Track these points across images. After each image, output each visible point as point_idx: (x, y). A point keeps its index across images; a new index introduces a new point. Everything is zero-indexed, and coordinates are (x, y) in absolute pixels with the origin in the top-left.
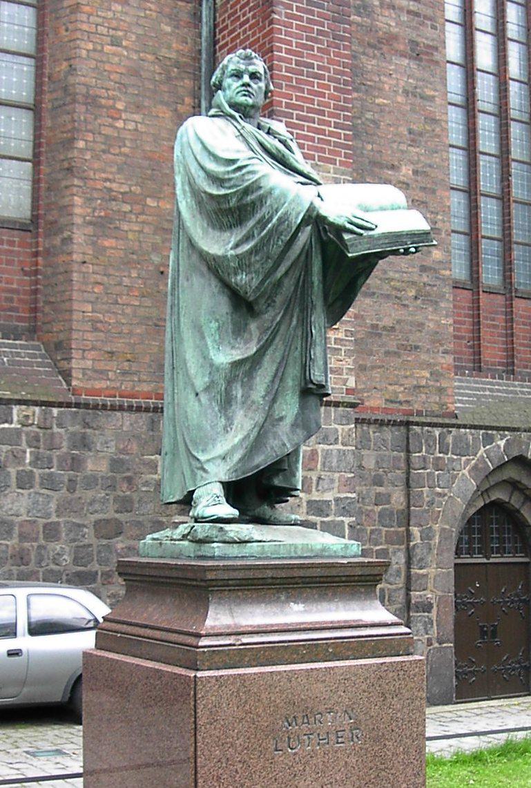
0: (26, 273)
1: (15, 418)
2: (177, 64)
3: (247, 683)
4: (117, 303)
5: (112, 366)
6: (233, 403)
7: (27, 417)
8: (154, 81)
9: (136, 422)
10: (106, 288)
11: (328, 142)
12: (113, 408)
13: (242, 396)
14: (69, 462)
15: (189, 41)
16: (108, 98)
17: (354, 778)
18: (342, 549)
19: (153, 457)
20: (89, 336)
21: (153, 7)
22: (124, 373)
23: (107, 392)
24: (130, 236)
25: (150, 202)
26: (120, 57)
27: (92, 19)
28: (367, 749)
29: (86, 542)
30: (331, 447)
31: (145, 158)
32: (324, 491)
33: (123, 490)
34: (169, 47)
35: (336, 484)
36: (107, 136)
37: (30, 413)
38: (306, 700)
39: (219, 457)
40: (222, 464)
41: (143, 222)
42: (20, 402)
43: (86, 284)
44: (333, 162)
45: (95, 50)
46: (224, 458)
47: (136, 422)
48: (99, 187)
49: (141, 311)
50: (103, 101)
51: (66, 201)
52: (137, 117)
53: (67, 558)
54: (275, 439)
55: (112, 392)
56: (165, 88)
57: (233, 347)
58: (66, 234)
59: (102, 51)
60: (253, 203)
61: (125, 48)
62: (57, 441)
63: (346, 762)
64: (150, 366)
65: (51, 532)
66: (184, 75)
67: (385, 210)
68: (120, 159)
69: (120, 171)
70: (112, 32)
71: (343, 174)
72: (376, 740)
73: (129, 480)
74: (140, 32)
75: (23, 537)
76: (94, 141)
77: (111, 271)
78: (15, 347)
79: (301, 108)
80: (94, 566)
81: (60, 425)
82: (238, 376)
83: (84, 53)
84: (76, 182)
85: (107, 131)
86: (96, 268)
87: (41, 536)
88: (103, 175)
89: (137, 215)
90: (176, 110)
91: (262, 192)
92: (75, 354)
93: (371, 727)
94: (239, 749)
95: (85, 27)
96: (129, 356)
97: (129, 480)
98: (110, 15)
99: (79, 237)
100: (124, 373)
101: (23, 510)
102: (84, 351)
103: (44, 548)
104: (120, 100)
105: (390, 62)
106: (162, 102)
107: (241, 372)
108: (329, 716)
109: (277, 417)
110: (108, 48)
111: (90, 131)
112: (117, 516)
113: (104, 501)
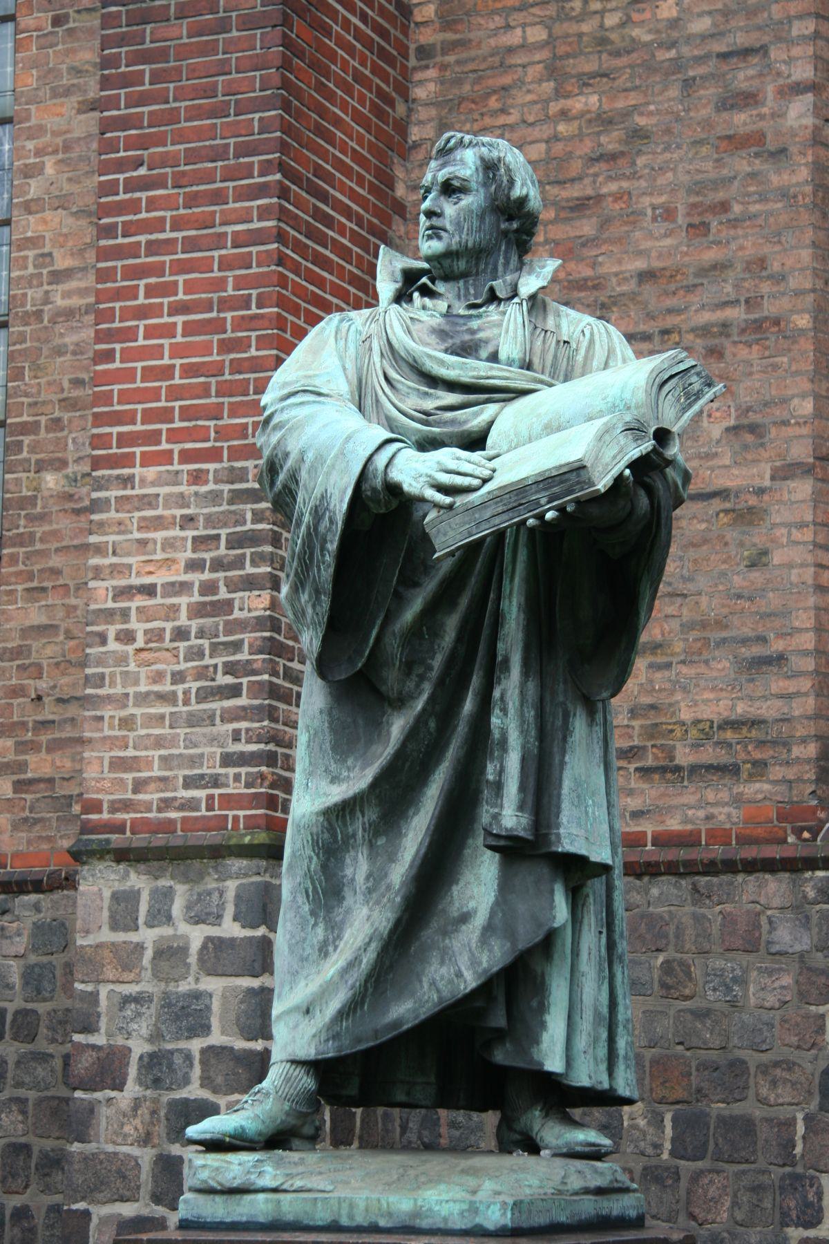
6: (347, 892)
13: (367, 878)
18: (462, 1213)
39: (296, 1009)
46: (308, 1011)
54: (442, 963)
57: (335, 780)
60: (285, 486)
67: (559, 429)
82: (354, 836)
107: (358, 826)
109: (456, 914)
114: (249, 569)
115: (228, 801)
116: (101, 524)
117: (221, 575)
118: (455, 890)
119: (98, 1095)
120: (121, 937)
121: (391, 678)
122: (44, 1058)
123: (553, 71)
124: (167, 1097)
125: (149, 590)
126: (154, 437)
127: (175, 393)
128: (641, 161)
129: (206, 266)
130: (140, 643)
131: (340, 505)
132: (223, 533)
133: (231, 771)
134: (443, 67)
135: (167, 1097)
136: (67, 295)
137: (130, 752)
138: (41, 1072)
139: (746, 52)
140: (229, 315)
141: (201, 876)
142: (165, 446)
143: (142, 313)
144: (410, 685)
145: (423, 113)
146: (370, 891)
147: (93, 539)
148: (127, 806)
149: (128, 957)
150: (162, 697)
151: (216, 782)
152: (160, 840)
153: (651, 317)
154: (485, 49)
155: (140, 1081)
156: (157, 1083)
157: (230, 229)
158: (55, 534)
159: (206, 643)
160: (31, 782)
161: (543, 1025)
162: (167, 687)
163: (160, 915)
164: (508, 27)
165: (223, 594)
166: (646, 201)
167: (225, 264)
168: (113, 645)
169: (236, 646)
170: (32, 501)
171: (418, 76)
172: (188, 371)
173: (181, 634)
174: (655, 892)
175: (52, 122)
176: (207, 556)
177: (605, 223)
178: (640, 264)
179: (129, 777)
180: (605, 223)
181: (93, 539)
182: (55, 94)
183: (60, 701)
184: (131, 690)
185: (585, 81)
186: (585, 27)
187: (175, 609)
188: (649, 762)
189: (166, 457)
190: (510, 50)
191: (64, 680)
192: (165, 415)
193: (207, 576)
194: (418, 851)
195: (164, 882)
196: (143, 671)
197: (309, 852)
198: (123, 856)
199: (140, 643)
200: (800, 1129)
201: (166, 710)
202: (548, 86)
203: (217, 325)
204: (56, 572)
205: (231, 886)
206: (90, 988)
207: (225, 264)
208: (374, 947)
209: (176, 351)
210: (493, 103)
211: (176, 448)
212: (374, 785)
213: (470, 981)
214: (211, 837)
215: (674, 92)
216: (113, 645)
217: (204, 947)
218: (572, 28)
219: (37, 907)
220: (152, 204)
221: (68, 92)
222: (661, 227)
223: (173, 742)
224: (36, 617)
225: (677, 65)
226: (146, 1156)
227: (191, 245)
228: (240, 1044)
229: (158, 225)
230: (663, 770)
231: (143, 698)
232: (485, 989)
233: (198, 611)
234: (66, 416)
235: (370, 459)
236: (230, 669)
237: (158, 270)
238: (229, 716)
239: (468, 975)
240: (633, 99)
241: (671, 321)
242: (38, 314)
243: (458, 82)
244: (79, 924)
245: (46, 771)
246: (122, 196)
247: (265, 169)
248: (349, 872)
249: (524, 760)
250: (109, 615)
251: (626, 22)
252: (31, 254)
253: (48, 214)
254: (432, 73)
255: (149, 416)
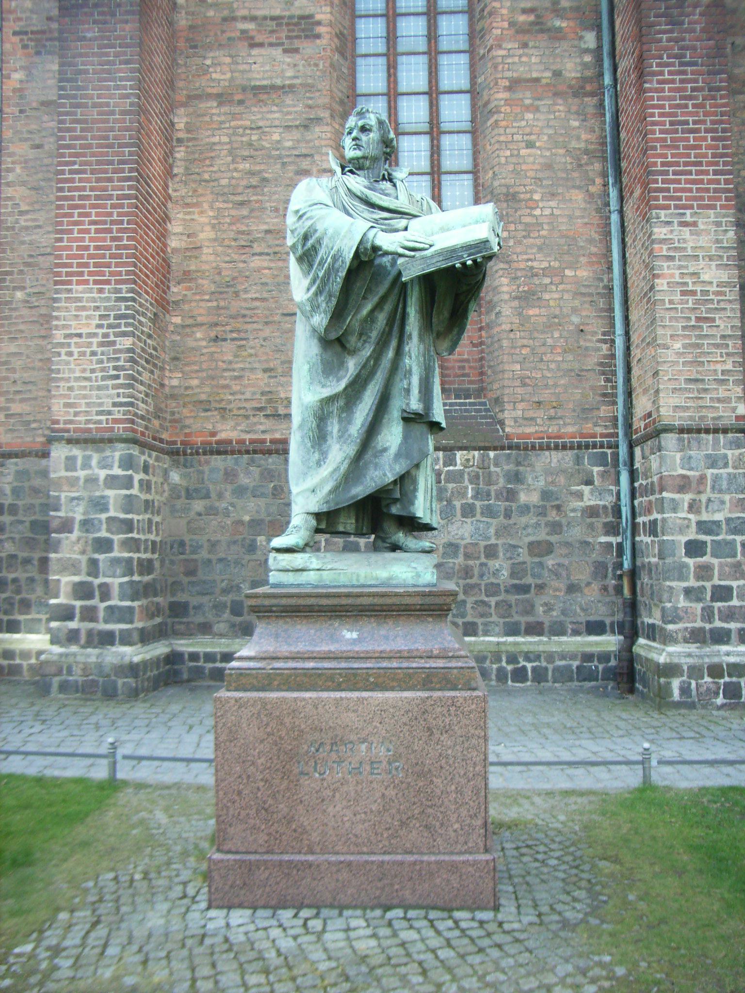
0: (474, 345)
1: (458, 462)
2: (586, 152)
3: (269, 706)
4: (542, 360)
5: (540, 414)
6: (329, 438)
7: (468, 460)
8: (566, 171)
9: (563, 459)
10: (533, 349)
11: (707, 190)
12: (541, 448)
14: (505, 494)
15: (597, 129)
16: (526, 192)
17: (394, 811)
19: (579, 488)
20: (519, 390)
21: (561, 108)
22: (551, 418)
23: (536, 436)
24: (552, 303)
25: (568, 272)
26: (533, 159)
27: (508, 131)
28: (409, 784)
29: (521, 559)
30: (721, 471)
31: (562, 237)
32: (714, 512)
33: (553, 516)
34: (578, 138)
35: (728, 505)
36: (526, 224)
37: (470, 457)
38: (335, 728)
39: (308, 490)
40: (312, 496)
41: (563, 291)
42: (461, 449)
43: (515, 348)
44: (714, 207)
45: (512, 155)
47: (563, 459)
48: (522, 266)
49: (565, 366)
50: (522, 196)
51: (496, 283)
52: (553, 204)
53: (505, 573)
54: (376, 470)
55: (541, 435)
56: (575, 175)
57: (323, 386)
58: (498, 309)
59: (518, 155)
61: (539, 148)
62: (494, 478)
63: (383, 795)
64: (574, 411)
65: (491, 552)
66: (594, 160)
67: (448, 230)
68: (539, 242)
69: (540, 249)
70: (526, 138)
71: (724, 216)
72: (421, 775)
73: (558, 508)
74: (551, 132)
75: (467, 556)
76: (516, 230)
77: (536, 335)
78: (465, 404)
79: (677, 164)
80: (529, 580)
81: (496, 465)
83: (503, 160)
84: (502, 266)
85: (528, 220)
86: (522, 334)
87: (483, 556)
88: (525, 257)
89: (557, 285)
90: (587, 191)
91: (317, 235)
92: (507, 406)
93: (414, 761)
94: (261, 768)
95: (502, 138)
96: (554, 404)
97: (558, 508)
98: (524, 123)
99: (507, 310)
100: (551, 418)
101: (467, 535)
102: (515, 403)
103: (485, 565)
104: (536, 192)
105: (205, 58)
106: (574, 187)
107: (335, 408)
108: (363, 747)
110: (523, 152)
111: (512, 222)
112: (548, 538)
113: (537, 525)
114: (123, 329)
115: (115, 421)
116: (58, 308)
117: (111, 330)
118: (380, 438)
119: (62, 536)
120: (69, 474)
121: (353, 341)
122: (21, 522)
123: (231, 152)
124: (91, 536)
125: (80, 335)
126: (81, 274)
127: (91, 257)
128: (266, 190)
129: (104, 206)
130: (76, 356)
131: (349, 255)
132: (112, 313)
133: (117, 409)
134: (187, 147)
135: (91, 536)
136: (26, 220)
137: (72, 401)
138: (20, 527)
139: (305, 156)
140: (115, 227)
141: (103, 451)
142: (86, 277)
143: (76, 223)
144: (360, 344)
145: (179, 163)
146: (340, 437)
147: (55, 314)
148: (71, 422)
149: (73, 482)
150: (86, 379)
151: (109, 413)
152: (86, 435)
153: (269, 247)
154: (204, 142)
155: (80, 530)
156: (87, 531)
157: (115, 193)
158: (21, 316)
159: (104, 357)
160: (12, 415)
161: (415, 497)
162: (88, 375)
163: (86, 465)
164: (214, 135)
165: (112, 338)
166: (268, 204)
167: (113, 206)
168: (64, 357)
169: (118, 359)
170: (11, 302)
171: (177, 149)
172: (97, 248)
173: (94, 354)
174: (270, 460)
175: (18, 151)
176: (105, 322)
177: (252, 211)
178: (265, 227)
179: (72, 410)
180: (252, 211)
181: (55, 314)
182: (21, 140)
183: (24, 383)
184: (72, 376)
185: (244, 158)
186: (244, 139)
187: (91, 343)
188: (269, 412)
189: (86, 282)
190: (214, 144)
191: (25, 375)
192: (86, 265)
193: (105, 330)
194: (366, 419)
195: (88, 453)
196: (78, 368)
197: (312, 419)
198: (69, 441)
199: (76, 356)
200: (323, 544)
201: (87, 384)
202: (230, 159)
203: (110, 231)
204: (22, 331)
205: (117, 455)
206: (56, 494)
207: (113, 206)
208: (347, 462)
209: (92, 240)
210: (208, 162)
211: (92, 278)
212: (345, 389)
213: (390, 478)
214: (107, 435)
215: (279, 166)
216: (64, 357)
217: (106, 479)
218: (239, 139)
219: (16, 464)
220: (81, 180)
221: (26, 140)
222: (273, 214)
223: (90, 397)
224: (13, 348)
225: (280, 157)
226: (84, 559)
227: (97, 198)
228: (122, 516)
229: (83, 189)
230: (274, 416)
231: (77, 379)
232: (395, 482)
233: (101, 344)
234: (26, 269)
235: (365, 234)
236: (115, 368)
237: (83, 207)
238: (115, 387)
239: (389, 475)
240: (262, 167)
241: (277, 249)
242: (13, 228)
243: (193, 153)
244: (51, 469)
245: (19, 411)
246: (67, 176)
247: (131, 170)
248: (329, 428)
249: (420, 379)
250: (62, 345)
251: (260, 139)
252: (10, 203)
253: (17, 188)
254: (182, 149)
255: (79, 265)
